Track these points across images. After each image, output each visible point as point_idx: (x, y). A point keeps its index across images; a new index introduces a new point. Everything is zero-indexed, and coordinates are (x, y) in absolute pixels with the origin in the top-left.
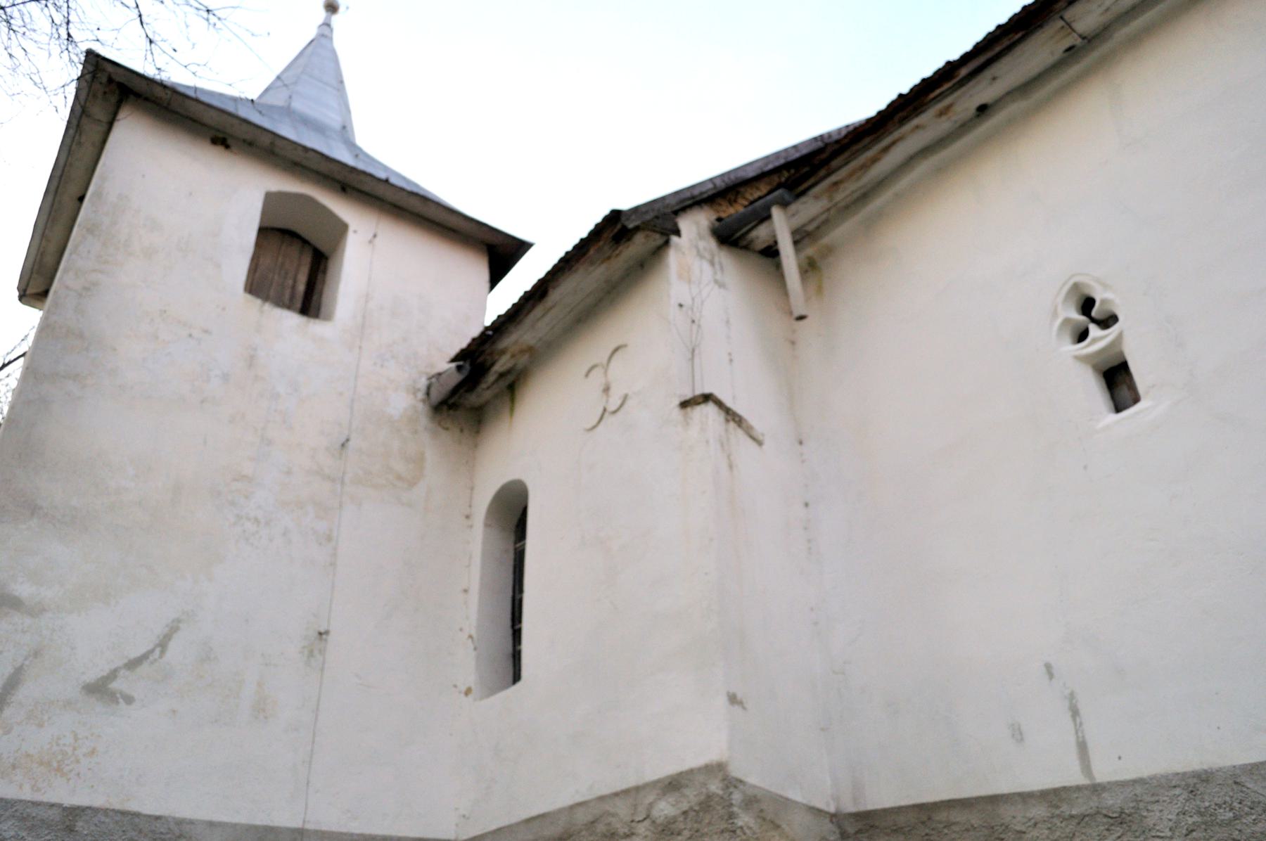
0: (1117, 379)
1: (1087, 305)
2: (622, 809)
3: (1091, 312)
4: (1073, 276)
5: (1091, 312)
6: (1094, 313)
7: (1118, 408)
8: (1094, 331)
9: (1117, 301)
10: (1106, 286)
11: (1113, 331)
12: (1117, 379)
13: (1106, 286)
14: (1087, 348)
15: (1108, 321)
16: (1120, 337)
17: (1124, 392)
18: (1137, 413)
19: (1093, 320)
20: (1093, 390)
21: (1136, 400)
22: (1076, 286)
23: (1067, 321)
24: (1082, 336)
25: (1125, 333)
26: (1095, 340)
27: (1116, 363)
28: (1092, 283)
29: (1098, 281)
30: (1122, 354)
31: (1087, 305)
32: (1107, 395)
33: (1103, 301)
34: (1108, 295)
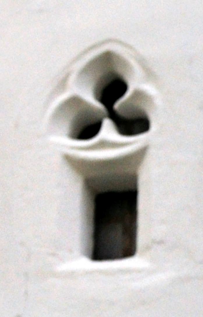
0: (112, 216)
1: (112, 88)
2: (112, 55)
3: (112, 100)
4: (109, 40)
5: (112, 100)
6: (117, 106)
7: (99, 253)
8: (108, 131)
9: (158, 101)
10: (150, 74)
11: (135, 142)
12: (112, 216)
13: (150, 74)
14: (88, 151)
15: (134, 124)
16: (140, 155)
17: (116, 234)
18: (122, 271)
19: (113, 116)
20: (69, 213)
21: (129, 251)
22: (107, 58)
23: (75, 101)
24: (87, 130)
25: (152, 153)
26: (103, 145)
27: (120, 187)
28: (133, 62)
29: (142, 62)
30: (134, 179)
31: (112, 88)
32: (90, 229)
33: (139, 95)
34: (149, 89)
